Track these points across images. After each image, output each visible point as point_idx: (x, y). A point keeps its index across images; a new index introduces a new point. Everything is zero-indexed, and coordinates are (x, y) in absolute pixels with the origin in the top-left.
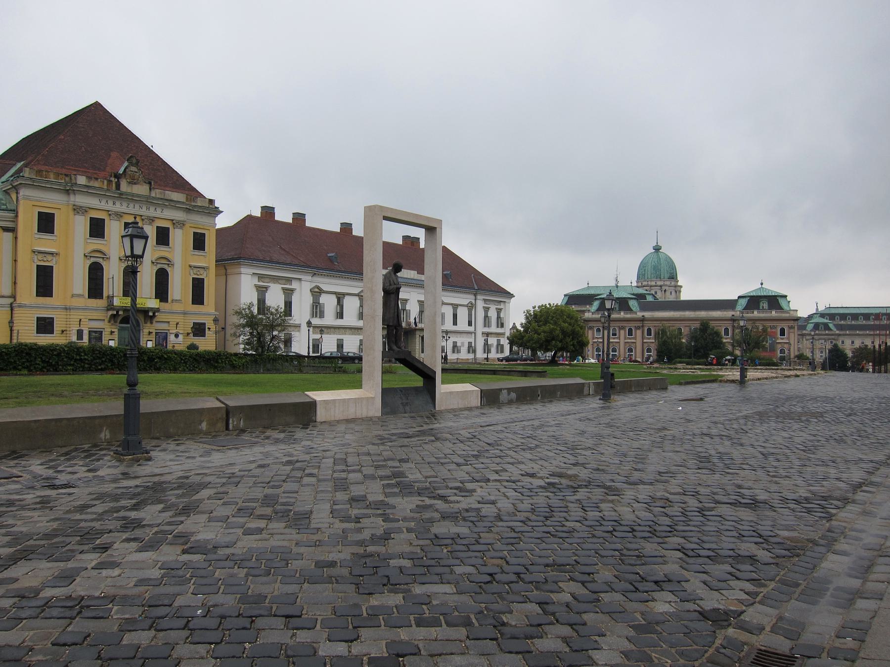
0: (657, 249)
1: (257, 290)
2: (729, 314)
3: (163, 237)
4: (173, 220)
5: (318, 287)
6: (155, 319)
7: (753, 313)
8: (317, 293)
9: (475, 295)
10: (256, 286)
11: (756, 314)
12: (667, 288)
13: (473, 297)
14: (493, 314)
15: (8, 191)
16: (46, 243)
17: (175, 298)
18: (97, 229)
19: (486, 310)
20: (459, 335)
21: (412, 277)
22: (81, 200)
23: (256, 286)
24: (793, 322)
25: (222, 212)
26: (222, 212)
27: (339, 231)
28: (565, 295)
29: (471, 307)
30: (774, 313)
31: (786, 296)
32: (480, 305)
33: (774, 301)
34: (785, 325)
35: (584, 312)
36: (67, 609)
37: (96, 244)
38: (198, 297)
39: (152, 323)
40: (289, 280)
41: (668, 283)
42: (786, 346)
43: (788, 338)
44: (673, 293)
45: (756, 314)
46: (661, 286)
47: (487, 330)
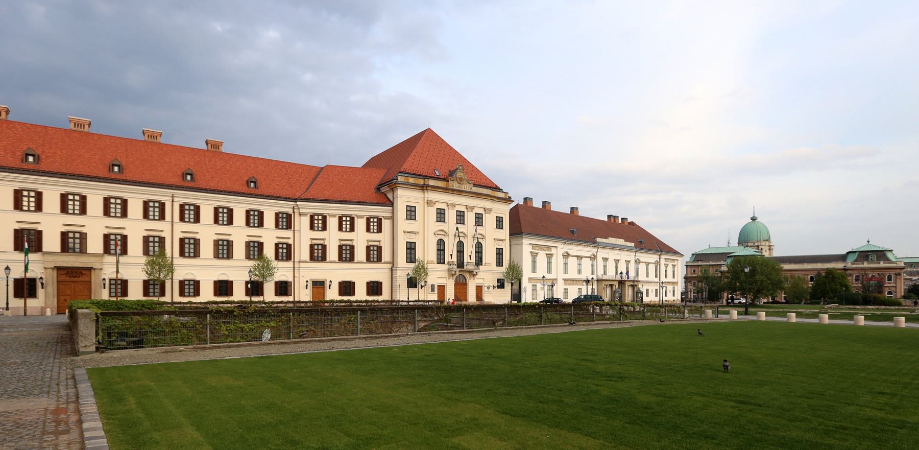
0: (754, 219)
1: (547, 257)
2: (840, 265)
3: (479, 220)
4: (485, 208)
5: (567, 253)
6: (477, 276)
7: (863, 264)
8: (567, 255)
9: (660, 255)
10: (531, 252)
11: (866, 265)
12: (762, 247)
13: (658, 257)
14: (670, 269)
15: (385, 193)
16: (411, 225)
17: (302, 259)
18: (441, 216)
19: (666, 266)
20: (649, 284)
21: (621, 244)
22: (432, 196)
23: (531, 252)
24: (899, 270)
25: (514, 201)
26: (514, 201)
27: (569, 213)
28: (693, 255)
29: (657, 264)
30: (882, 264)
31: (891, 251)
32: (663, 262)
33: (881, 254)
34: (892, 273)
35: (720, 265)
36: (49, 263)
37: (441, 226)
38: (499, 263)
39: (474, 279)
40: (550, 248)
41: (763, 244)
42: (893, 289)
43: (896, 283)
44: (768, 251)
45: (866, 265)
46: (758, 246)
47: (534, 275)
